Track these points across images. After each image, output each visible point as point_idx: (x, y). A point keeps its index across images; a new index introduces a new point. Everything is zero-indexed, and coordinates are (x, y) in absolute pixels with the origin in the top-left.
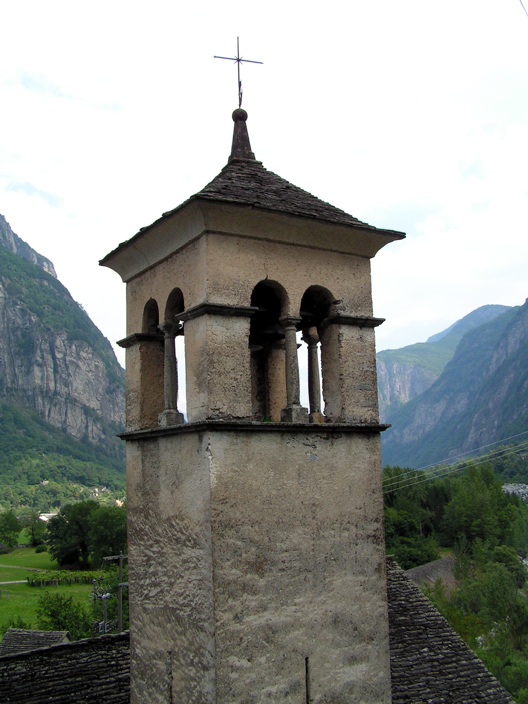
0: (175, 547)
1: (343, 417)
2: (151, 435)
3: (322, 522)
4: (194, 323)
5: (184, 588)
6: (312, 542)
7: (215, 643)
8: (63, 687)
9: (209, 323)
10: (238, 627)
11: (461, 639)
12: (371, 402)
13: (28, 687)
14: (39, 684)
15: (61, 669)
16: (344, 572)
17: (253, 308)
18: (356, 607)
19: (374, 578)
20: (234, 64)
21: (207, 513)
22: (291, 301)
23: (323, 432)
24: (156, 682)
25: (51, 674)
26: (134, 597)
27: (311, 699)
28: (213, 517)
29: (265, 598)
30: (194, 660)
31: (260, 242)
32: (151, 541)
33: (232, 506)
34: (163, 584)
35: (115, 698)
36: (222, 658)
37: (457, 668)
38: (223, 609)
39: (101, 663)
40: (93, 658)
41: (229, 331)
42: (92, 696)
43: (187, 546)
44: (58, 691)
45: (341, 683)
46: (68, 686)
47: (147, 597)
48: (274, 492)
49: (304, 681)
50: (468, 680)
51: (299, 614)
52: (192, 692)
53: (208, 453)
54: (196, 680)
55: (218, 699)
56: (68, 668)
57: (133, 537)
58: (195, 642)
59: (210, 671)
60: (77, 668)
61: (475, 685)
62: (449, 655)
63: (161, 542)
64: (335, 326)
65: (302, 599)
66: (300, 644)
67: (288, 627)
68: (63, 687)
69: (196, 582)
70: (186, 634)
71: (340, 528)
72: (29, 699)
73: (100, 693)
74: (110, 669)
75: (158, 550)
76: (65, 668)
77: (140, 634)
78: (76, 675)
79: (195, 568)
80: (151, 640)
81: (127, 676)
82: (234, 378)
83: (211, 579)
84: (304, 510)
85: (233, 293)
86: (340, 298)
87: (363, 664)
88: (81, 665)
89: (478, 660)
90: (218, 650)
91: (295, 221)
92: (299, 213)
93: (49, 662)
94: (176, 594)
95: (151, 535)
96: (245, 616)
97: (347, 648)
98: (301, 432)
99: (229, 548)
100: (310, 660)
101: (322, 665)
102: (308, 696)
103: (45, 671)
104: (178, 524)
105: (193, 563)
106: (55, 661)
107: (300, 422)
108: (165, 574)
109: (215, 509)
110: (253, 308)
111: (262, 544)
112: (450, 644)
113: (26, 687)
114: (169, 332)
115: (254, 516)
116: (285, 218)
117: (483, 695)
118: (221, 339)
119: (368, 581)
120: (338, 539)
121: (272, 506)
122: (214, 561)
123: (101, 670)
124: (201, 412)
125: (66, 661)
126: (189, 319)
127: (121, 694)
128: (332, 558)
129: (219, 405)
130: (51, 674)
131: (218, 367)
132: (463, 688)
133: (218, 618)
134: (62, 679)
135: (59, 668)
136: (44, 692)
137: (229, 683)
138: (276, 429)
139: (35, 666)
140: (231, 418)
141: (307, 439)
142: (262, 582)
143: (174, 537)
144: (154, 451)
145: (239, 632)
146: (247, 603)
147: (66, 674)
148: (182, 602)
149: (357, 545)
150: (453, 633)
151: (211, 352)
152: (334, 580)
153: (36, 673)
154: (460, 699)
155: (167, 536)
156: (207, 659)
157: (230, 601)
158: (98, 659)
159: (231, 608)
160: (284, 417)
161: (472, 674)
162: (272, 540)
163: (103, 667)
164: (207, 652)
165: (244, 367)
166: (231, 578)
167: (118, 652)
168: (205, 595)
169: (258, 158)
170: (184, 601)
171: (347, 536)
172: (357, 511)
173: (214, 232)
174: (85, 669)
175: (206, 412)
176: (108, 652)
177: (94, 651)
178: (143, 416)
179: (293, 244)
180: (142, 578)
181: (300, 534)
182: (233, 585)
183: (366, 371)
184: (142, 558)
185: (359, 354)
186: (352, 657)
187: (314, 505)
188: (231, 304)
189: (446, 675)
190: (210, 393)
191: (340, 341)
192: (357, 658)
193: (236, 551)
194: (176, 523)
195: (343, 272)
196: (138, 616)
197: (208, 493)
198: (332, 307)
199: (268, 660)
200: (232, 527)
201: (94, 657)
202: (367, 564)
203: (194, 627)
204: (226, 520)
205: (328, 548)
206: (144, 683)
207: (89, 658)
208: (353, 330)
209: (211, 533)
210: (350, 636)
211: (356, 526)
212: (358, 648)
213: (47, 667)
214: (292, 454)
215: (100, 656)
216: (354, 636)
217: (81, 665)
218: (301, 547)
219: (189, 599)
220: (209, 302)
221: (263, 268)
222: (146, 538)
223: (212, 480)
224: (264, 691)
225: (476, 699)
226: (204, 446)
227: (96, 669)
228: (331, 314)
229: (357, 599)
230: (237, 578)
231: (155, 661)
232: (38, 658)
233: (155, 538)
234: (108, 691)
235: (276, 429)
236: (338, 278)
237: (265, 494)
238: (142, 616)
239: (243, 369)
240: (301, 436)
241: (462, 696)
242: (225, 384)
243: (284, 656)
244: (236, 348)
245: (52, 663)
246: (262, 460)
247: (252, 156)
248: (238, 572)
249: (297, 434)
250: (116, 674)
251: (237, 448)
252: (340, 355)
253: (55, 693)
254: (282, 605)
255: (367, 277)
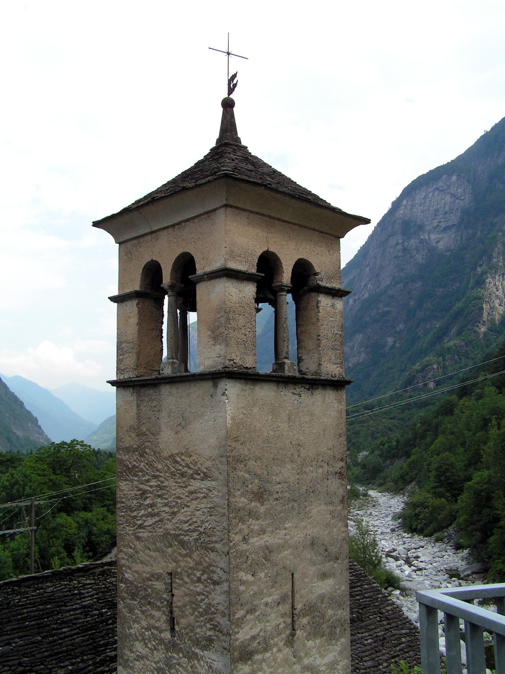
0: (179, 480)
1: (319, 372)
2: (153, 382)
3: (305, 460)
4: (208, 284)
5: (190, 516)
6: (297, 477)
7: (229, 560)
8: (36, 613)
9: (227, 284)
10: (244, 547)
11: (361, 568)
12: (339, 360)
13: (6, 614)
14: (15, 611)
15: (31, 598)
16: (319, 502)
17: (258, 274)
18: (326, 532)
19: (339, 508)
20: (224, 56)
21: (222, 449)
22: (285, 271)
23: (306, 383)
24: (152, 600)
25: (24, 603)
26: (124, 527)
27: (295, 608)
28: (228, 452)
29: (264, 523)
30: (202, 577)
31: (264, 218)
32: (147, 476)
33: (242, 444)
34: (161, 514)
35: (83, 622)
36: (234, 573)
37: (361, 591)
38: (235, 532)
39: (65, 592)
40: (58, 588)
41: (241, 293)
42: (63, 621)
43: (195, 479)
44: (33, 617)
45: (316, 595)
46: (41, 613)
47: (141, 526)
48: (272, 433)
49: (291, 593)
50: (371, 601)
51: (288, 537)
52: (198, 605)
53: (225, 397)
54: (204, 594)
55: (231, 608)
56: (37, 597)
57: (124, 474)
58: (204, 562)
59: (222, 585)
60: (45, 597)
61: (377, 604)
62: (354, 581)
63: (161, 477)
64: (313, 294)
65: (290, 524)
66: (288, 562)
67: (281, 547)
68: (36, 613)
69: (205, 510)
70: (192, 556)
71: (317, 465)
72: (8, 625)
73: (70, 618)
74: (74, 598)
75: (156, 484)
76: (35, 597)
77: (131, 560)
78: (45, 603)
79: (205, 497)
80: (145, 564)
81: (90, 603)
82: (245, 334)
83: (226, 506)
84: (292, 449)
85: (244, 260)
86: (320, 271)
87: (331, 579)
88: (49, 594)
89: (376, 584)
90: (231, 566)
91: (294, 202)
92: (299, 196)
93: (20, 592)
94: (179, 522)
95: (147, 471)
96: (250, 538)
97: (320, 566)
98: (291, 383)
99: (240, 480)
100: (295, 575)
101: (303, 580)
102: (293, 606)
103: (18, 599)
104: (183, 460)
105: (202, 493)
106: (25, 591)
107: (290, 374)
108: (166, 505)
109: (230, 446)
110: (258, 274)
111: (262, 477)
112: (353, 572)
113: (3, 614)
114: (173, 291)
115: (257, 453)
116: (287, 199)
117: (384, 611)
118: (235, 299)
119: (335, 510)
120: (314, 474)
121: (269, 445)
122: (229, 491)
123: (66, 598)
124: (217, 362)
125: (34, 590)
126: (204, 280)
127: (88, 619)
128: (311, 491)
129: (233, 356)
130: (24, 603)
131: (233, 324)
132: (368, 607)
133: (231, 539)
134: (34, 607)
135: (29, 597)
136: (21, 618)
137: (238, 595)
138: (275, 379)
139: (8, 595)
140: (242, 368)
141: (295, 389)
142: (262, 509)
143: (178, 472)
144: (154, 396)
145: (246, 551)
146: (251, 527)
147: (37, 602)
148: (187, 528)
149: (328, 480)
150: (354, 563)
151: (228, 310)
152: (312, 509)
153: (10, 601)
154: (367, 615)
155: (169, 471)
156: (219, 574)
157: (240, 524)
158: (62, 589)
159: (241, 531)
160: (276, 369)
161: (373, 595)
162: (270, 474)
163: (68, 596)
164: (219, 569)
165: (251, 324)
166: (240, 505)
167: (79, 583)
168: (218, 521)
169: (243, 143)
170: (190, 527)
171: (321, 472)
172: (329, 451)
173: (231, 206)
174: (53, 597)
175: (223, 361)
176: (70, 583)
177: (57, 581)
178: (138, 366)
179: (288, 222)
180: (135, 510)
181: (289, 470)
182: (242, 511)
183: (336, 334)
184: (135, 492)
185: (332, 319)
186: (323, 573)
187: (299, 444)
188: (243, 269)
189: (355, 597)
190: (227, 345)
191: (318, 307)
192: (327, 574)
193: (244, 483)
194: (182, 459)
195: (321, 249)
196: (129, 544)
197: (224, 432)
198: (312, 278)
199: (266, 575)
200: (242, 462)
201: (58, 587)
202: (334, 496)
203: (202, 549)
204: (238, 456)
205: (308, 481)
206: (136, 603)
207: (55, 588)
208: (327, 298)
209: (226, 466)
210: (322, 556)
211: (328, 464)
212: (328, 565)
213: (19, 596)
214: (284, 400)
215: (64, 586)
216: (325, 555)
217: (49, 594)
218: (290, 480)
219: (196, 525)
220: (227, 266)
221: (266, 240)
222: (140, 474)
223: (228, 420)
224: (263, 601)
225: (379, 615)
226: (220, 390)
227: (62, 598)
228: (310, 284)
229: (328, 525)
230: (245, 506)
231: (150, 583)
232: (9, 588)
233: (152, 473)
234: (76, 616)
235: (275, 379)
236: (318, 254)
237: (265, 434)
238: (133, 544)
239: (251, 326)
240: (291, 386)
241: (369, 612)
242: (238, 338)
243: (277, 572)
244: (246, 308)
245: (23, 593)
246: (263, 405)
247: (238, 140)
248: (246, 500)
249: (288, 384)
250: (80, 601)
251: (246, 394)
252: (318, 319)
253: (30, 618)
254: (276, 529)
255: (338, 254)
